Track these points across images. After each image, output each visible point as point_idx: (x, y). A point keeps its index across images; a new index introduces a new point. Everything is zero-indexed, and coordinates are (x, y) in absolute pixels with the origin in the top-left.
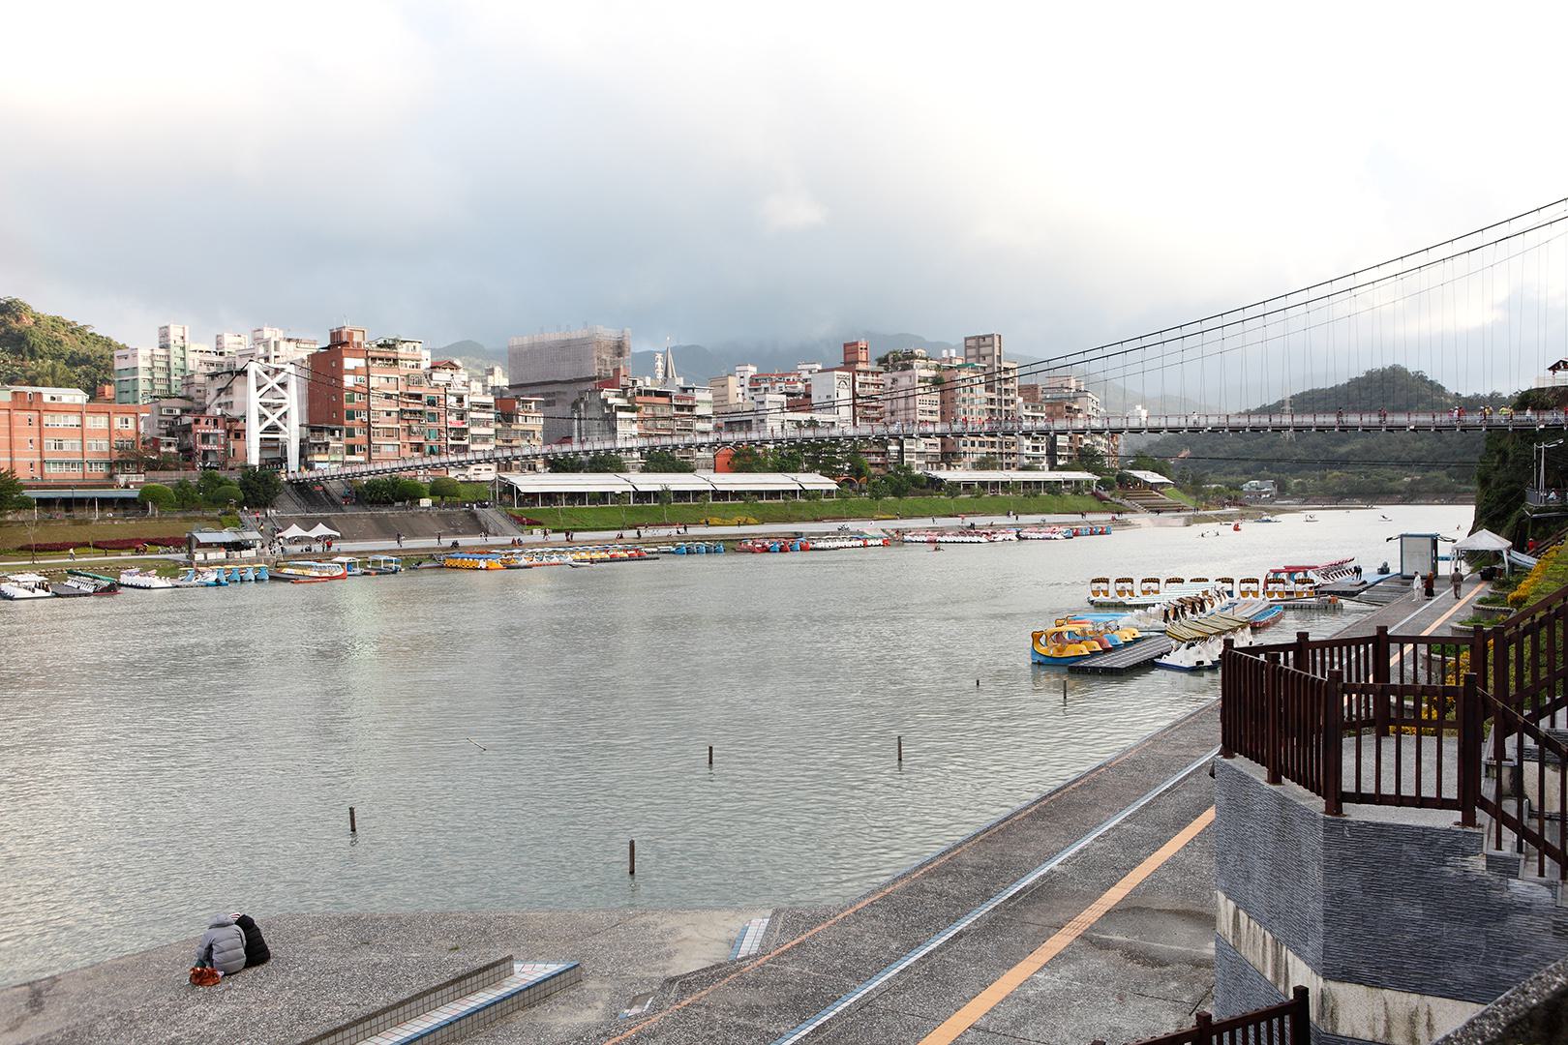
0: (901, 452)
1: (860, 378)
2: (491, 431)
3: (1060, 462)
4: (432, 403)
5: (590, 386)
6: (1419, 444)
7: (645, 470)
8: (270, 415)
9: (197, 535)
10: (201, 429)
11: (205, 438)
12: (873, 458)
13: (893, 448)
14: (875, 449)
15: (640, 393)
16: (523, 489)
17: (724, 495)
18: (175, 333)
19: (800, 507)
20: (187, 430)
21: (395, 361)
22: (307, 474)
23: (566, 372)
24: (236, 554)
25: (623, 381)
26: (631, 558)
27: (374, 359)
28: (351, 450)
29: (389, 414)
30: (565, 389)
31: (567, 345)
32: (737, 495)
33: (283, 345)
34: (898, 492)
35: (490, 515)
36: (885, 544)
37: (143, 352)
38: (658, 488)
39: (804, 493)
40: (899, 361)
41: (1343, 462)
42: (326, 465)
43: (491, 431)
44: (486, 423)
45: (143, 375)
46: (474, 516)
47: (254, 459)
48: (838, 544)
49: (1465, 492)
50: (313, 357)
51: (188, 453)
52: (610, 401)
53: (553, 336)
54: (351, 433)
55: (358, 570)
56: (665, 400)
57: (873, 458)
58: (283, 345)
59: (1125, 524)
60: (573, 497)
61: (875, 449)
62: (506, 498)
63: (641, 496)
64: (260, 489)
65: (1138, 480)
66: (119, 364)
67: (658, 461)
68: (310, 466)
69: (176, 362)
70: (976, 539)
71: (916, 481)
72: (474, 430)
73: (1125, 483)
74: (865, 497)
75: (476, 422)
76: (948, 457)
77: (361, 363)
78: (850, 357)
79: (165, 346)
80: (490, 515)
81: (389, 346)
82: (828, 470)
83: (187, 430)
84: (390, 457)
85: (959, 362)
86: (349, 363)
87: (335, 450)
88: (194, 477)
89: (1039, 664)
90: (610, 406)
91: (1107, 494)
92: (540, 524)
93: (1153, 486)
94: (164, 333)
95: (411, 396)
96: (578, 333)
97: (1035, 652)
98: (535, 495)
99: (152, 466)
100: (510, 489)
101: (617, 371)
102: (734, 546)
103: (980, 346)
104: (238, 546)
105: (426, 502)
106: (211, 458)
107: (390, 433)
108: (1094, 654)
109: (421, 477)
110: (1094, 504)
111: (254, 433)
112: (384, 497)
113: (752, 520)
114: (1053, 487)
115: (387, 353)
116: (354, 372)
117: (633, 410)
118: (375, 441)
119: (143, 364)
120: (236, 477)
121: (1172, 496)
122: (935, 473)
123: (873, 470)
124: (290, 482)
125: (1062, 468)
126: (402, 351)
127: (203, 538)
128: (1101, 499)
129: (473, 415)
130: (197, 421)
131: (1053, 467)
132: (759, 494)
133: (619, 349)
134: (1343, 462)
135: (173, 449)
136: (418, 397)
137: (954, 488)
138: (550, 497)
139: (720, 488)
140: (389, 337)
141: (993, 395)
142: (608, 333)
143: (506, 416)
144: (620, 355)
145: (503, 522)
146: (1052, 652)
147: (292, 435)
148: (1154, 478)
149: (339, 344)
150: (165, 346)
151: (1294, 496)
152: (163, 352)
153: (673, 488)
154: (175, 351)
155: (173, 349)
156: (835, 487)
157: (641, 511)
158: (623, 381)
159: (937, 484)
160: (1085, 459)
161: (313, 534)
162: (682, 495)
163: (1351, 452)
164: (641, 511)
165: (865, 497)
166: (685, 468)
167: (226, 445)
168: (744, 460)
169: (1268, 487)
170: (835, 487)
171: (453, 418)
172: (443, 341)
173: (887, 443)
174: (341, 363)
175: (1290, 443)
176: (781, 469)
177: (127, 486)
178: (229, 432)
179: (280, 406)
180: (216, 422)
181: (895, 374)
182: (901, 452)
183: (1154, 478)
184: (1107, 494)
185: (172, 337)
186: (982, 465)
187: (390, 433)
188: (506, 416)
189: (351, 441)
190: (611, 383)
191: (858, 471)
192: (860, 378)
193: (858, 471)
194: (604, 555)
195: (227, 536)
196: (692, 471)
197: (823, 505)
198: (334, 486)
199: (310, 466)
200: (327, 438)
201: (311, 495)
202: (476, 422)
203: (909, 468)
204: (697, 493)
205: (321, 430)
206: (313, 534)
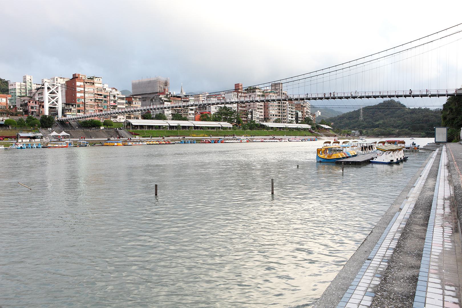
0: (252, 117)
1: (240, 94)
2: (124, 107)
3: (299, 122)
4: (105, 97)
5: (157, 94)
6: (399, 122)
7: (173, 119)
8: (53, 101)
9: (20, 134)
10: (31, 104)
11: (32, 108)
12: (243, 119)
13: (250, 116)
14: (244, 116)
15: (172, 96)
16: (133, 124)
17: (197, 128)
18: (28, 78)
19: (221, 132)
20: (26, 105)
21: (93, 83)
22: (64, 118)
23: (149, 91)
24: (33, 140)
25: (166, 93)
26: (166, 144)
27: (86, 83)
28: (79, 111)
29: (91, 100)
30: (149, 95)
31: (150, 82)
32: (201, 128)
33: (59, 79)
34: (251, 128)
35: (123, 132)
36: (247, 142)
37: (18, 84)
38: (177, 125)
39: (222, 128)
40: (251, 90)
41: (377, 126)
42: (69, 116)
43: (124, 107)
44: (123, 104)
45: (18, 91)
46: (117, 132)
47: (47, 113)
48: (232, 141)
49: (414, 134)
50: (67, 82)
51: (26, 112)
52: (162, 99)
53: (145, 79)
54: (79, 106)
55: (72, 145)
56: (180, 99)
57: (243, 119)
58: (59, 79)
59: (319, 139)
60: (150, 127)
61: (244, 116)
62: (128, 127)
63: (171, 127)
64: (47, 123)
65: (322, 127)
66: (10, 87)
67: (176, 117)
68: (65, 116)
69: (28, 87)
70: (276, 141)
71: (257, 125)
72: (119, 106)
73: (318, 127)
74: (241, 130)
75: (119, 104)
76: (266, 119)
77: (82, 84)
78: (237, 88)
79: (25, 82)
80: (123, 132)
81: (91, 79)
82: (230, 121)
83: (26, 105)
84: (91, 113)
85: (269, 91)
86: (78, 84)
87: (73, 111)
88: (25, 118)
89: (320, 162)
90: (162, 100)
91: (313, 131)
92: (138, 135)
93: (327, 129)
94: (25, 78)
95: (98, 95)
96: (153, 78)
97: (318, 157)
98: (137, 126)
99: (12, 115)
100: (129, 124)
101: (165, 89)
102: (199, 141)
103: (276, 86)
104: (34, 138)
105: (102, 128)
106: (34, 113)
107: (92, 106)
108: (344, 158)
109: (102, 121)
110: (310, 134)
111: (47, 105)
112: (89, 126)
113: (206, 135)
114: (297, 129)
115: (91, 81)
116: (80, 86)
117: (169, 101)
118: (87, 109)
119: (18, 87)
120: (39, 118)
121: (331, 132)
122: (262, 123)
123: (244, 122)
124: (58, 121)
125: (300, 123)
126: (96, 80)
127: (22, 135)
128: (312, 132)
129: (118, 101)
130: (29, 102)
131: (297, 123)
132: (209, 128)
133: (166, 84)
134: (377, 126)
135: (21, 111)
136: (101, 95)
137: (268, 128)
138: (142, 127)
139: (196, 125)
140: (91, 75)
141: (280, 104)
142: (163, 79)
143: (130, 103)
144: (166, 86)
145: (126, 134)
146: (326, 157)
147: (60, 107)
148: (327, 127)
149: (75, 78)
150: (25, 82)
151: (364, 135)
152: (24, 84)
153: (181, 125)
154: (28, 84)
155: (27, 83)
156: (232, 126)
157: (171, 132)
158: (166, 93)
159: (263, 127)
160: (307, 121)
161: (61, 134)
162: (184, 127)
163: (380, 124)
164: (171, 132)
165: (241, 130)
166: (185, 119)
167: (39, 110)
168: (204, 117)
169: (357, 133)
170: (232, 126)
171: (112, 102)
172: (110, 81)
173: (247, 115)
174: (75, 84)
175: (362, 121)
176: (215, 120)
177: (3, 121)
178: (40, 106)
179: (50, 93)
180: (36, 102)
181: (250, 94)
182: (252, 117)
183: (327, 127)
184: (313, 131)
185: (27, 79)
186: (276, 121)
187: (92, 106)
188: (130, 103)
189: (79, 108)
190: (163, 93)
191: (239, 122)
192: (240, 94)
193: (239, 122)
194: (158, 143)
195: (31, 134)
196: (188, 120)
197: (228, 132)
198: (72, 123)
199: (65, 116)
200: (71, 107)
201: (64, 124)
202: (119, 104)
203: (254, 122)
204: (189, 127)
205: (69, 105)
206: (61, 134)
